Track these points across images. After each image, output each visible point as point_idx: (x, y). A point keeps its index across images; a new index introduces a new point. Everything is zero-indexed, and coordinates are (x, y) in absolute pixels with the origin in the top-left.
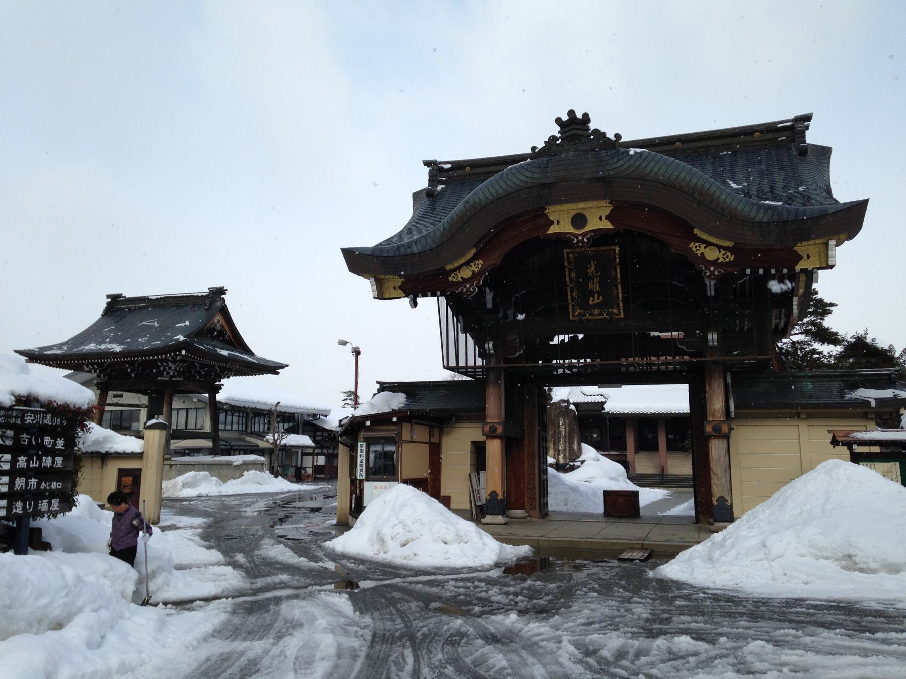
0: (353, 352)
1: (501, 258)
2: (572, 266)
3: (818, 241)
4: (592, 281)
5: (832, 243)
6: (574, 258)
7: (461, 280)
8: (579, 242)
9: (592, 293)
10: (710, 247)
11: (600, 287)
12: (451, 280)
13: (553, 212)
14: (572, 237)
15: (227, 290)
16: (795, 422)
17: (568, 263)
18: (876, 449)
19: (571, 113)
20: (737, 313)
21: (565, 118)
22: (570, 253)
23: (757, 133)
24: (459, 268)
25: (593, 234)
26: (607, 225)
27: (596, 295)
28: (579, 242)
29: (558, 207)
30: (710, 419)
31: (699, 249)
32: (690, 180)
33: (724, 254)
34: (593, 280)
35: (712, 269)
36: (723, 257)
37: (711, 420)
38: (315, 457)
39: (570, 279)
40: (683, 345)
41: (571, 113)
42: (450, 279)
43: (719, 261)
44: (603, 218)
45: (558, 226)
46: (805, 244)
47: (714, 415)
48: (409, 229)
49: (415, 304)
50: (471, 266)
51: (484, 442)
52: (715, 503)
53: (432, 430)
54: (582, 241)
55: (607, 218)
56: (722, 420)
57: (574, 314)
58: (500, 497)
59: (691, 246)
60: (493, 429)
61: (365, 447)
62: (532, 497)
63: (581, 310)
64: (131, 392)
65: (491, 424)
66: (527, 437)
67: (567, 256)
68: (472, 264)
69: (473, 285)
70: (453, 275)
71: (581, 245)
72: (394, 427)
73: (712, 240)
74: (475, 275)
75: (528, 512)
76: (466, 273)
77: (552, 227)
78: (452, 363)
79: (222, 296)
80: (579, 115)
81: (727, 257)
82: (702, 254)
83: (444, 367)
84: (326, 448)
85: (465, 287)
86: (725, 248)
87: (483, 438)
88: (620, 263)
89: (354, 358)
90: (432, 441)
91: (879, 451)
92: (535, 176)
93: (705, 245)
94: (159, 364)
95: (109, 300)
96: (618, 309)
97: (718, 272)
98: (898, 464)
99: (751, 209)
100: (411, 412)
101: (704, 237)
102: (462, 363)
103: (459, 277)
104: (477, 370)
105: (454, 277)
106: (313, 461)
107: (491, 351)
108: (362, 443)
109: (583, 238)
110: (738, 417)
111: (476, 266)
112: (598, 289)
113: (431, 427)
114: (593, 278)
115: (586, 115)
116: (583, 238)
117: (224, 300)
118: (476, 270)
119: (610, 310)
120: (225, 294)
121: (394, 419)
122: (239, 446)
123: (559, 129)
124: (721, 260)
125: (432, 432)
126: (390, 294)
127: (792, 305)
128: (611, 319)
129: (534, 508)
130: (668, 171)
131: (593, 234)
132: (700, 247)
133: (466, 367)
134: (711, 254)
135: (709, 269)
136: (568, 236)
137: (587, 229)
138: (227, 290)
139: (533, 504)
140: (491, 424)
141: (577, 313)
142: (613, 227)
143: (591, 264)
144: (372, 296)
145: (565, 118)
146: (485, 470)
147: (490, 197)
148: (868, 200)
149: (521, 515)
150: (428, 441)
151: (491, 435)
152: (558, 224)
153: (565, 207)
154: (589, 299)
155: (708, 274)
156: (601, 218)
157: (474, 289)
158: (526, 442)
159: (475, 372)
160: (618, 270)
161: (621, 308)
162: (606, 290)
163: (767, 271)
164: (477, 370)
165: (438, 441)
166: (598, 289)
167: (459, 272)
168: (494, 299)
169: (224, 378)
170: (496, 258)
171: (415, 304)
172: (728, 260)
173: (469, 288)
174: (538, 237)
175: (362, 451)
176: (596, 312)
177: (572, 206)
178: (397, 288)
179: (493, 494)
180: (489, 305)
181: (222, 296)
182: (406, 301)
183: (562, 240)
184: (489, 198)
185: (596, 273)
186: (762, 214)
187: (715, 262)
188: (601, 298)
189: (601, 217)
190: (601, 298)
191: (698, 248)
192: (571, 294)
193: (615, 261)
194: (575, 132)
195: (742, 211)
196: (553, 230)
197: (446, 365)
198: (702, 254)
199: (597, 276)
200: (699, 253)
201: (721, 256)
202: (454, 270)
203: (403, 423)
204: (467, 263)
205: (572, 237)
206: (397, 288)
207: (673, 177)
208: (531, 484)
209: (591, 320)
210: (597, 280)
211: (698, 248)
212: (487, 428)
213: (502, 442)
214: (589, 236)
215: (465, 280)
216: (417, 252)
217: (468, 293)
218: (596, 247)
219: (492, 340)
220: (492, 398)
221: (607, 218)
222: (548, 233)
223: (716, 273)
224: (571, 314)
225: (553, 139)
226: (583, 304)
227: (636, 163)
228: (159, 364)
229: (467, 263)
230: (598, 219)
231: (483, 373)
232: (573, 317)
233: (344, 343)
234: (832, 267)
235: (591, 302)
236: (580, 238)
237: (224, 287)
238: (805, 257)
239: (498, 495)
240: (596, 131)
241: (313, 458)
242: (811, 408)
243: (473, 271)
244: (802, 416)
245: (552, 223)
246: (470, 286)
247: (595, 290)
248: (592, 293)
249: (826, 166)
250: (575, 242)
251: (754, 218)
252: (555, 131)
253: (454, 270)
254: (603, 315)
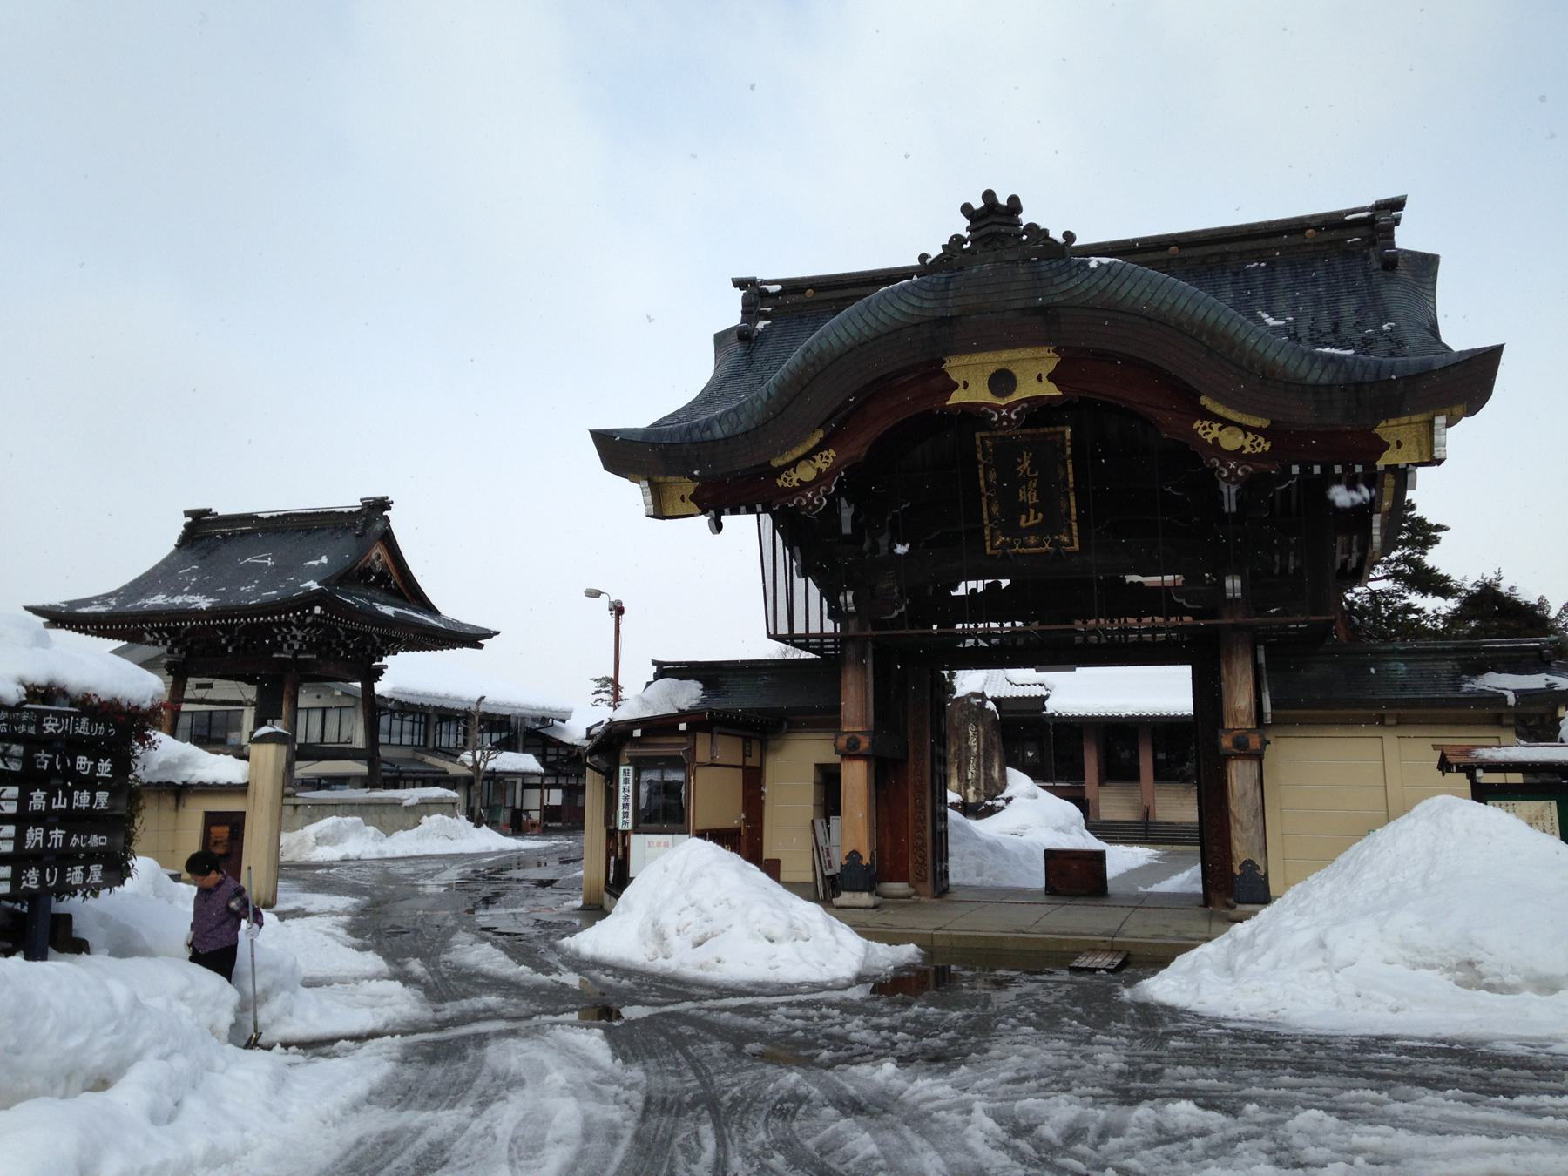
0: (610, 610)
1: (867, 447)
2: (989, 461)
3: (1416, 418)
4: (1024, 487)
5: (1440, 421)
6: (994, 447)
7: (797, 485)
8: (1001, 419)
9: (1024, 507)
10: (1229, 428)
11: (1038, 497)
12: (780, 485)
13: (957, 368)
14: (990, 411)
15: (392, 502)
16: (1375, 731)
17: (983, 455)
18: (1516, 778)
19: (989, 196)
20: (1275, 541)
21: (978, 204)
22: (986, 438)
23: (1310, 231)
24: (794, 464)
25: (1026, 405)
26: (1051, 390)
27: (1032, 511)
28: (1001, 419)
29: (965, 359)
30: (1229, 725)
31: (1209, 432)
32: (1194, 312)
33: (1253, 441)
34: (1027, 484)
35: (1232, 465)
36: (1252, 446)
37: (1231, 727)
38: (546, 791)
39: (987, 482)
40: (1181, 598)
41: (989, 196)
42: (780, 483)
43: (1245, 452)
44: (1044, 378)
45: (965, 392)
46: (1392, 422)
47: (1235, 720)
48: (708, 397)
49: (717, 527)
50: (815, 460)
51: (838, 766)
52: (1238, 872)
53: (747, 744)
54: (1008, 418)
55: (1051, 377)
56: (1249, 727)
57: (994, 544)
58: (866, 860)
59: (1195, 426)
60: (853, 743)
61: (631, 774)
62: (920, 860)
63: (1006, 536)
64: (226, 679)
65: (850, 735)
66: (911, 756)
67: (982, 443)
68: (817, 457)
69: (819, 493)
70: (783, 476)
71: (1005, 424)
72: (682, 740)
73: (1232, 415)
74: (821, 477)
75: (913, 887)
76: (807, 473)
77: (955, 394)
78: (783, 629)
79: (385, 513)
80: (1002, 200)
81: (1259, 444)
82: (1215, 440)
83: (769, 636)
84: (564, 775)
85: (805, 496)
86: (1254, 430)
87: (836, 759)
88: (1073, 456)
89: (613, 621)
90: (747, 764)
91: (1522, 782)
92: (926, 304)
93: (1219, 425)
94: (276, 630)
95: (189, 519)
96: (1070, 535)
97: (1242, 471)
98: (1554, 803)
99: (1300, 363)
100: (711, 714)
101: (1219, 410)
102: (799, 629)
103: (795, 479)
104: (825, 641)
105: (785, 480)
106: (542, 799)
107: (849, 609)
108: (626, 768)
109: (1009, 412)
110: (1278, 722)
111: (824, 460)
112: (1035, 500)
113: (747, 740)
114: (1026, 481)
115: (1014, 200)
116: (1009, 412)
117: (387, 519)
118: (824, 467)
119: (1056, 537)
120: (389, 509)
121: (683, 727)
122: (414, 772)
123: (967, 223)
124: (1248, 450)
125: (747, 749)
126: (674, 510)
127: (1371, 528)
128: (1058, 553)
129: (924, 880)
130: (1156, 296)
131: (1026, 405)
132: (1211, 428)
133: (807, 636)
134: (1231, 440)
135: (1227, 467)
136: (983, 409)
137: (1015, 397)
138: (392, 502)
139: (923, 874)
140: (850, 735)
141: (998, 543)
142: (1060, 393)
143: (1022, 457)
144: (644, 513)
145: (978, 204)
146: (839, 814)
147: (849, 342)
148: (1502, 346)
149: (902, 892)
150: (741, 764)
151: (850, 753)
152: (965, 388)
153: (978, 358)
154: (1020, 518)
155: (1225, 475)
156: (1039, 378)
157: (820, 500)
158: (911, 766)
159: (822, 644)
160: (1070, 467)
161: (1075, 533)
162: (1049, 501)
163: (1327, 469)
164: (825, 641)
165: (758, 764)
166: (1035, 500)
167: (795, 471)
168: (854, 518)
169: (388, 654)
170: (858, 447)
171: (717, 527)
172: (1259, 450)
173: (812, 499)
174: (931, 411)
175: (626, 781)
176: (1032, 540)
177: (990, 356)
178: (687, 498)
179: (854, 856)
180: (847, 529)
181: (385, 513)
182: (702, 521)
183: (973, 415)
184: (847, 343)
185: (1031, 472)
186: (1320, 371)
187: (1237, 454)
188: (1040, 515)
189: (1040, 375)
190: (1040, 515)
191: (1208, 430)
192: (989, 510)
193: (1065, 453)
194: (994, 228)
195: (1284, 365)
196: (957, 398)
197: (772, 633)
198: (1215, 440)
199: (1033, 478)
200: (1209, 438)
201: (1247, 443)
202: (786, 467)
203: (698, 733)
204: (808, 456)
205: (990, 411)
206: (687, 498)
207: (1165, 307)
208: (920, 838)
209: (1023, 554)
210: (1033, 484)
211: (1208, 430)
212: (842, 742)
213: (868, 766)
214: (1019, 409)
215: (804, 485)
216: (722, 436)
217: (810, 508)
218: (1031, 428)
219: (851, 589)
220: (852, 690)
221: (1051, 377)
222: (948, 403)
223: (1239, 472)
224: (988, 543)
225: (957, 240)
226: (1010, 526)
227: (1101, 283)
228: (276, 630)
229: (808, 456)
230: (1035, 380)
231: (836, 646)
232: (992, 548)
233: (596, 594)
234: (1439, 462)
235: (1023, 524)
236: (1004, 412)
237: (387, 498)
238: (1394, 445)
239: (861, 858)
240: (1032, 227)
241: (542, 793)
242: (1403, 707)
243: (819, 470)
244: (1388, 721)
245: (955, 386)
246: (814, 496)
247: (1030, 503)
248: (1024, 507)
249: (1430, 287)
250: (996, 418)
251: (1305, 378)
252: (961, 226)
253: (786, 467)
254: (1044, 546)
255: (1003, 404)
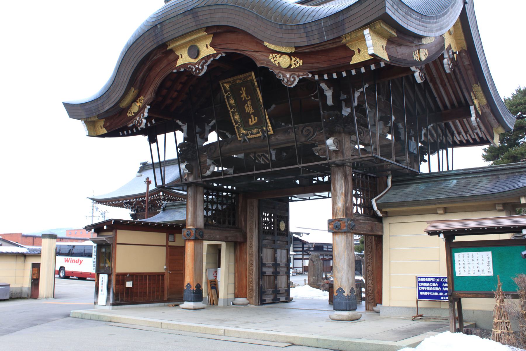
4: (246, 105)
6: (230, 87)
8: (196, 69)
9: (249, 116)
10: (283, 56)
26: (212, 51)
27: (252, 116)
33: (295, 61)
35: (288, 76)
38: (304, 261)
43: (292, 67)
44: (209, 46)
59: (301, 61)
62: (251, 288)
74: (141, 109)
75: (248, 300)
77: (178, 61)
81: (297, 62)
93: (280, 55)
94: (157, 202)
95: (142, 165)
98: (490, 253)
106: (303, 264)
111: (140, 101)
114: (246, 102)
116: (198, 65)
118: (141, 105)
129: (252, 297)
134: (284, 61)
137: (200, 57)
149: (241, 303)
150: (165, 244)
156: (207, 47)
158: (248, 244)
165: (184, 245)
170: (150, 94)
172: (298, 65)
176: (255, 131)
185: (248, 97)
199: (248, 100)
200: (276, 63)
208: (251, 278)
209: (252, 138)
210: (249, 103)
222: (176, 66)
224: (238, 134)
226: (245, 124)
228: (157, 202)
229: (135, 101)
230: (205, 48)
235: (251, 124)
236: (197, 66)
238: (356, 51)
241: (303, 261)
246: (139, 119)
250: (194, 70)
255: (195, 62)
